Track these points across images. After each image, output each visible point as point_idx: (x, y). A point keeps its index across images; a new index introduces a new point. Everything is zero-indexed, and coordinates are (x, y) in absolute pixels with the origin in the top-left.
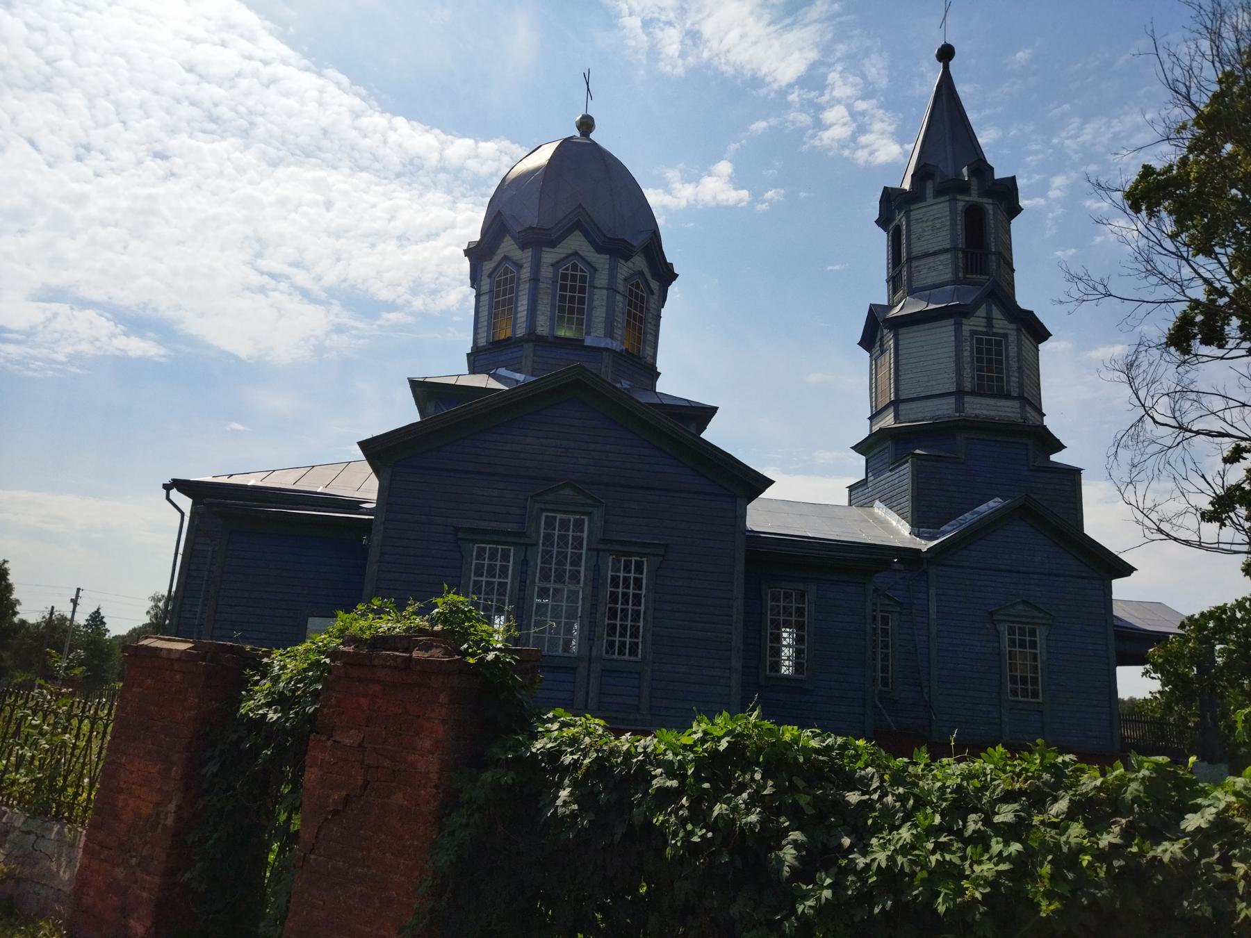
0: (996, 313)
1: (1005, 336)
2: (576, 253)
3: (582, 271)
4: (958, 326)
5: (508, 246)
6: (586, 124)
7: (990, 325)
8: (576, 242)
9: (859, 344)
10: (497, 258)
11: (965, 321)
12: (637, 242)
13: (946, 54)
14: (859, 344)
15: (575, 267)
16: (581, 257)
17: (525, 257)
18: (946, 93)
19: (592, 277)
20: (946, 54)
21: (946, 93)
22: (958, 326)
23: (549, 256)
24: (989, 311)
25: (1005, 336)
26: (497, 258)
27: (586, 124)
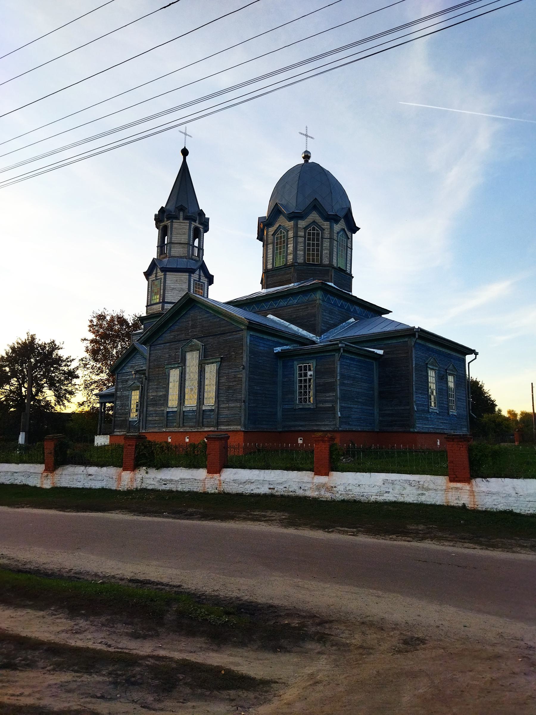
0: (202, 274)
1: (204, 283)
2: (314, 221)
3: (317, 230)
4: (190, 276)
5: (282, 221)
6: (307, 157)
7: (200, 279)
8: (314, 216)
9: (144, 273)
10: (277, 225)
11: (192, 275)
12: (342, 214)
13: (185, 152)
14: (144, 273)
15: (314, 229)
16: (316, 223)
17: (290, 224)
18: (184, 175)
19: (322, 233)
20: (185, 152)
21: (184, 175)
22: (190, 276)
23: (302, 224)
24: (200, 272)
25: (204, 283)
26: (277, 225)
27: (307, 157)
